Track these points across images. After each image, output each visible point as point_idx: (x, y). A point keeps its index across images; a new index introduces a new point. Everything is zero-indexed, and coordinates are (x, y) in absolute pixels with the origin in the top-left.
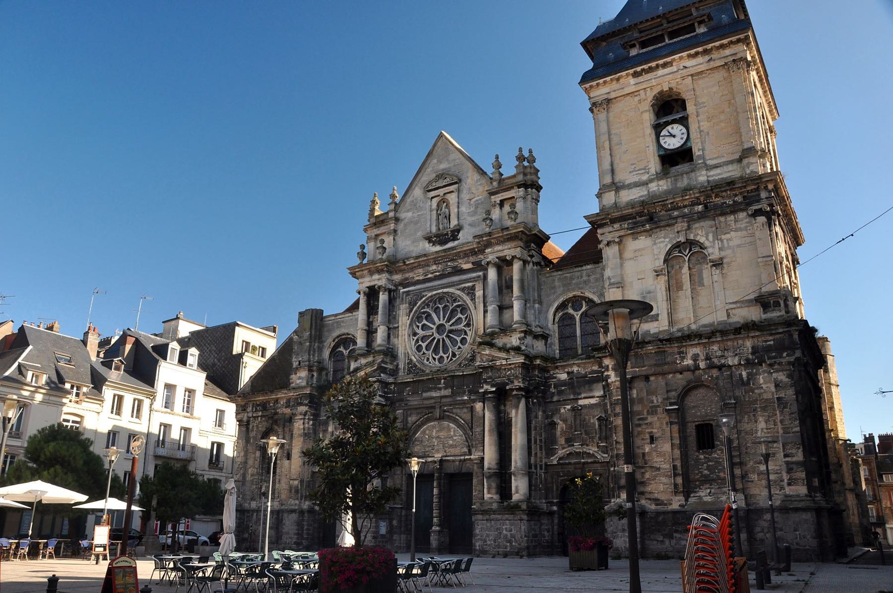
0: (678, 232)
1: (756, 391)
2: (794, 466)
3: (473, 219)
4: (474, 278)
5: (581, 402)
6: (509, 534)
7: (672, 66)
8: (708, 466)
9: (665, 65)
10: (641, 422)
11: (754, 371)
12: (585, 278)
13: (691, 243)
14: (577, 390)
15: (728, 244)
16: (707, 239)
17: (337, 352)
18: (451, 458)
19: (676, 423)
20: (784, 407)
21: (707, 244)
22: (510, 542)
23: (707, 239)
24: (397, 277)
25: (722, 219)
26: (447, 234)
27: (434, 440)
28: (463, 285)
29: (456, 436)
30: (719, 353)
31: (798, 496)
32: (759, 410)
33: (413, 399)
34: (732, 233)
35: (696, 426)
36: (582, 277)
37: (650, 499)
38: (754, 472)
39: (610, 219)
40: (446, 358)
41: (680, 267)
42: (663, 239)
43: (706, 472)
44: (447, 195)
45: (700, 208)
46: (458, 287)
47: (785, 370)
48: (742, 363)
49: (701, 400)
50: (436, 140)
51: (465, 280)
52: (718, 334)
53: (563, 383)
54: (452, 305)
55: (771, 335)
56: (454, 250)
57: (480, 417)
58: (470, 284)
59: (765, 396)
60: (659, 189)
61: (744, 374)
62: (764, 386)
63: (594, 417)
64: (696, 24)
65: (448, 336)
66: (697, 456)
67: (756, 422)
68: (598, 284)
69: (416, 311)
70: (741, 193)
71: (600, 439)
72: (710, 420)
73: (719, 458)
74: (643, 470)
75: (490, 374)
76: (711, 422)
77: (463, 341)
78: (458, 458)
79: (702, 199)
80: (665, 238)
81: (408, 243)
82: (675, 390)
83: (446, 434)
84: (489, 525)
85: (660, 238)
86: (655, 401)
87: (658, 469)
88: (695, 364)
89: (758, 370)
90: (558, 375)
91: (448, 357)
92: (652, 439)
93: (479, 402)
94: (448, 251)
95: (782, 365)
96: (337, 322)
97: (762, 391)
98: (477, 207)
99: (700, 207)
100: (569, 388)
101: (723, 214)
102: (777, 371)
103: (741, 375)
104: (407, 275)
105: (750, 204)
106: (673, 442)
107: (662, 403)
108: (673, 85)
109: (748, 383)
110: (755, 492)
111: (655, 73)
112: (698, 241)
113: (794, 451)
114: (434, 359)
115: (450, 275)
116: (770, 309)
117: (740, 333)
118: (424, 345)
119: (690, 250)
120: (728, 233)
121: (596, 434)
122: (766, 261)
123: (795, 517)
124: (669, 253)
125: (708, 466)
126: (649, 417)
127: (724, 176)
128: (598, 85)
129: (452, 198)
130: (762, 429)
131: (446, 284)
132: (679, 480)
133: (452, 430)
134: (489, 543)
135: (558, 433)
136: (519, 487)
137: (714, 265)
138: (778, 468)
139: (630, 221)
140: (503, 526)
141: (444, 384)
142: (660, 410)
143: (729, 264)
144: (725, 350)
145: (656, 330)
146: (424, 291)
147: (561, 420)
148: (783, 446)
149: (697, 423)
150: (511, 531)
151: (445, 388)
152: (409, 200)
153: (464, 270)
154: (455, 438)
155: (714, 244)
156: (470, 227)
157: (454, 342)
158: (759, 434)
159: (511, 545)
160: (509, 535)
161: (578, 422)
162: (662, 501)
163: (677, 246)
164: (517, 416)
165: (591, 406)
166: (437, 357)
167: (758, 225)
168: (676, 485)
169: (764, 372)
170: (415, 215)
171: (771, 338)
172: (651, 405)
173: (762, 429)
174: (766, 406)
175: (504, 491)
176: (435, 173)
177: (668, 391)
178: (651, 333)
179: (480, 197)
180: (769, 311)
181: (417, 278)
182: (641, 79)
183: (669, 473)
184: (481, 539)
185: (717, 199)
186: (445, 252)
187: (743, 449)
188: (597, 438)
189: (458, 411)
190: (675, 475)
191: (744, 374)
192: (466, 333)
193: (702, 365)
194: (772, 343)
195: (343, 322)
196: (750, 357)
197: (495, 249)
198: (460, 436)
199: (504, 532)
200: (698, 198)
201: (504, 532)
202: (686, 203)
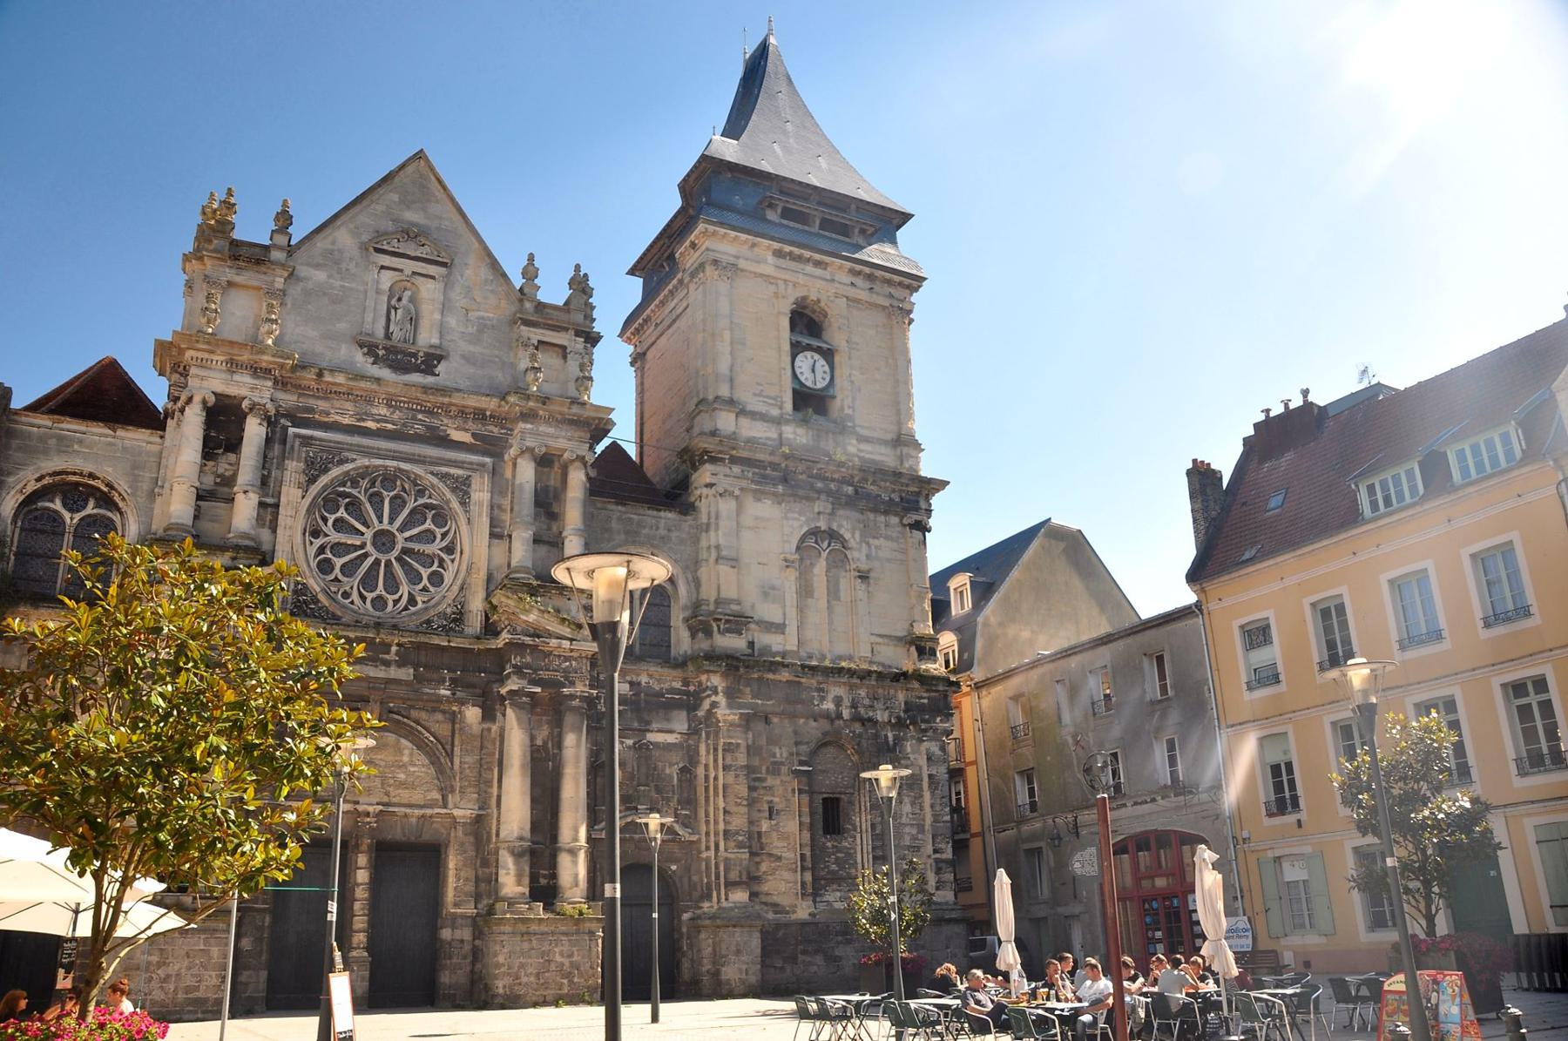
0: (819, 513)
2: (943, 865)
3: (472, 348)
4: (471, 463)
5: (652, 737)
6: (566, 962)
7: (825, 269)
8: (837, 858)
9: (818, 264)
10: (757, 784)
12: (662, 532)
13: (833, 535)
14: (646, 717)
16: (853, 537)
17: (36, 509)
19: (806, 792)
21: (852, 543)
22: (569, 976)
23: (853, 537)
24: (289, 399)
25: (871, 516)
26: (415, 355)
28: (444, 469)
29: (415, 765)
30: (867, 702)
36: (657, 528)
37: (766, 904)
39: (731, 456)
40: (390, 604)
41: (811, 564)
42: (796, 515)
43: (834, 867)
44: (417, 277)
45: (850, 490)
46: (432, 468)
48: (893, 721)
50: (410, 159)
51: (450, 461)
54: (416, 500)
55: (927, 691)
56: (445, 396)
57: (473, 736)
58: (459, 472)
60: (795, 439)
61: (890, 735)
63: (671, 765)
65: (398, 559)
66: (824, 843)
68: (683, 548)
69: (325, 488)
70: (900, 491)
71: (679, 802)
72: (840, 793)
75: (529, 659)
76: (843, 796)
77: (437, 579)
79: (856, 479)
81: (312, 333)
82: (807, 743)
83: (390, 758)
84: (526, 946)
85: (793, 512)
86: (778, 755)
87: (779, 858)
89: (905, 734)
91: (396, 602)
92: (772, 813)
93: (473, 705)
94: (433, 394)
96: (61, 438)
97: (909, 762)
98: (481, 331)
99: (850, 488)
101: (875, 510)
102: (930, 740)
103: (886, 736)
104: (312, 402)
105: (907, 510)
107: (787, 759)
108: (823, 298)
111: (802, 266)
112: (842, 536)
114: (363, 598)
115: (417, 439)
118: (339, 562)
119: (829, 545)
120: (877, 538)
121: (674, 793)
123: (947, 930)
124: (803, 539)
125: (837, 858)
126: (769, 777)
127: (877, 458)
128: (736, 238)
129: (429, 291)
131: (406, 453)
132: (808, 877)
133: (406, 752)
134: (524, 980)
137: (860, 577)
139: (757, 470)
140: (556, 945)
141: (396, 654)
142: (784, 769)
144: (875, 699)
146: (349, 450)
149: (825, 796)
150: (571, 956)
151: (401, 664)
152: (321, 243)
153: (452, 441)
154: (412, 769)
155: (861, 547)
157: (414, 578)
159: (571, 982)
160: (567, 964)
161: (643, 770)
162: (783, 907)
163: (815, 533)
164: (575, 749)
165: (668, 747)
166: (370, 596)
167: (914, 540)
168: (803, 884)
169: (912, 737)
170: (338, 283)
171: (925, 695)
172: (772, 759)
176: (393, 221)
177: (797, 744)
179: (491, 315)
181: (338, 418)
182: (781, 262)
183: (794, 866)
184: (508, 974)
185: (872, 487)
186: (425, 393)
188: (675, 800)
189: (423, 715)
190: (803, 869)
192: (441, 563)
193: (846, 714)
194: (926, 701)
195: (80, 442)
196: (902, 714)
197: (541, 429)
199: (558, 958)
200: (852, 477)
202: (836, 476)
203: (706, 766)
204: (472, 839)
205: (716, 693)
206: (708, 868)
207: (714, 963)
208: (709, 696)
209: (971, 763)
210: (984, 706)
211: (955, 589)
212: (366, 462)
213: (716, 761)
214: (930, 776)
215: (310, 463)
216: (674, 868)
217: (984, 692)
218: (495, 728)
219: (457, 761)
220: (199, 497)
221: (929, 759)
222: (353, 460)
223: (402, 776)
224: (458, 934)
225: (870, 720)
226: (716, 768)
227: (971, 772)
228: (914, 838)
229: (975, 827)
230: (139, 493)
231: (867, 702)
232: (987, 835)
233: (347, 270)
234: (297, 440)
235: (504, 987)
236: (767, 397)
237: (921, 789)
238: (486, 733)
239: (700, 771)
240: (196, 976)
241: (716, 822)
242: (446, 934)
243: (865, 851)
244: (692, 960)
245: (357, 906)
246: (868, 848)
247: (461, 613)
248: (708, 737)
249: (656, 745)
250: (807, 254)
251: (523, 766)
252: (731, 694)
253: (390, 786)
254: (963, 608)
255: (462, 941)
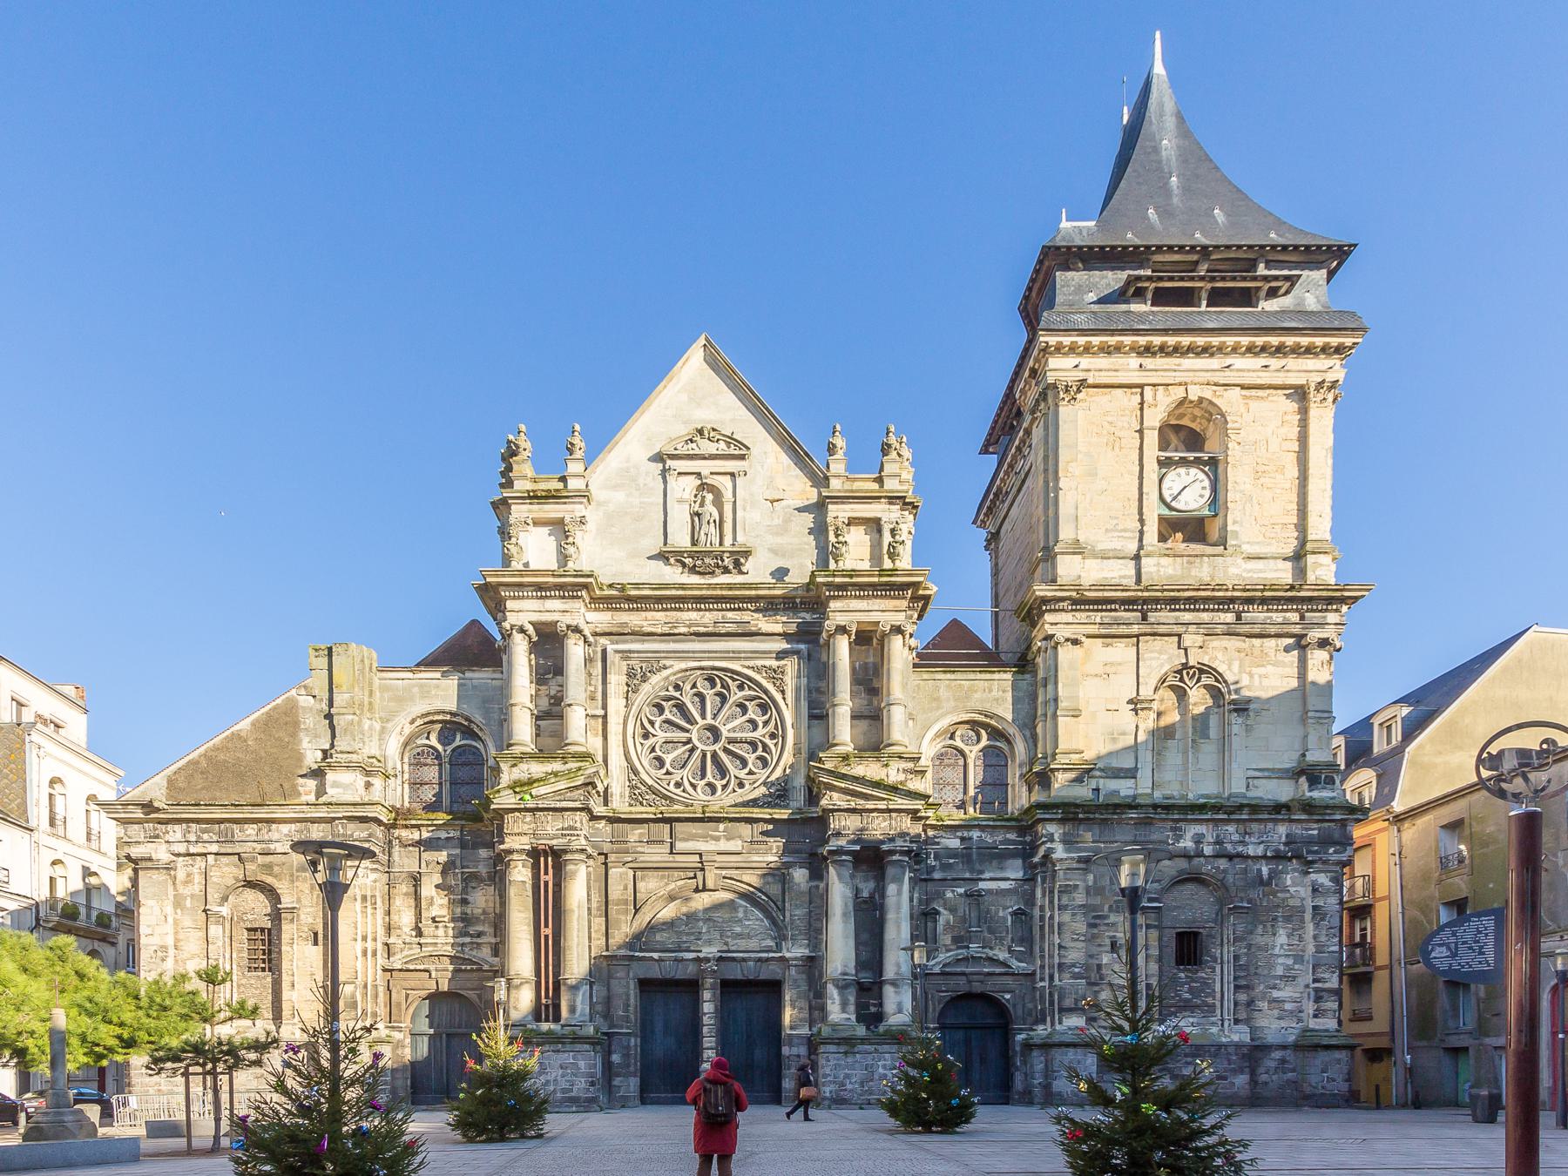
1: (1279, 895)
3: (779, 540)
5: (982, 885)
10: (1098, 921)
11: (1280, 867)
15: (1261, 683)
16: (1230, 669)
18: (741, 955)
19: (1155, 927)
20: (1323, 919)
23: (1230, 669)
27: (701, 924)
29: (749, 920)
30: (1236, 837)
31: (1327, 1031)
32: (1280, 919)
33: (650, 851)
34: (1269, 667)
35: (1179, 934)
36: (991, 691)
38: (1263, 999)
42: (1156, 655)
46: (747, 663)
47: (1330, 872)
49: (1188, 899)
52: (1246, 810)
53: (953, 853)
59: (1291, 902)
61: (1265, 870)
62: (1292, 890)
63: (1005, 908)
64: (1263, 294)
65: (726, 750)
67: (1275, 935)
71: (1013, 940)
73: (1208, 979)
74: (1096, 988)
76: (1201, 930)
78: (753, 955)
80: (1160, 653)
83: (727, 916)
85: (1152, 652)
88: (1197, 848)
90: (943, 840)
95: (1328, 864)
96: (421, 686)
97: (1288, 895)
100: (963, 863)
103: (1260, 871)
106: (1149, 952)
109: (1269, 883)
110: (1262, 1024)
113: (1326, 976)
116: (1320, 786)
117: (1279, 813)
120: (1263, 666)
121: (1007, 933)
122: (1320, 718)
126: (1112, 915)
130: (1282, 945)
133: (741, 910)
135: (940, 928)
136: (899, 1006)
137: (1236, 710)
138: (1298, 995)
143: (1257, 713)
144: (1246, 833)
145: (1131, 792)
147: (945, 909)
148: (1313, 968)
149: (1179, 930)
156: (772, 555)
158: (1277, 951)
169: (1294, 870)
171: (1315, 826)
173: (1282, 945)
174: (1291, 916)
175: (871, 1015)
176: (684, 423)
178: (1122, 794)
180: (1317, 789)
182: (1149, 362)
187: (1252, 970)
191: (1265, 870)
193: (1208, 850)
194: (1315, 832)
196: (1282, 847)
198: (757, 920)
199: (881, 1070)
201: (881, 1070)
203: (1042, 908)
204: (804, 976)
205: (1052, 840)
206: (1042, 997)
207: (1046, 1077)
208: (1044, 843)
209: (1382, 899)
210: (1404, 839)
211: (1381, 724)
212: (683, 665)
213: (1051, 902)
214: (1315, 908)
215: (631, 675)
216: (1008, 996)
217: (1407, 825)
218: (822, 885)
219: (787, 914)
220: (538, 718)
221: (1315, 890)
222: (671, 666)
223: (738, 929)
224: (795, 1051)
225: (1239, 855)
226: (1052, 909)
227: (1381, 912)
228: (1288, 968)
229: (1381, 958)
230: (492, 723)
231: (1236, 837)
232: (1396, 966)
233: (645, 485)
234: (617, 655)
235: (831, 1092)
236: (1125, 530)
237: (1302, 921)
238: (813, 890)
239: (1037, 912)
240: (568, 1081)
241: (1051, 956)
242: (785, 1050)
243: (1225, 980)
244: (1026, 1074)
245: (705, 1029)
246: (1229, 976)
247: (785, 790)
248: (1043, 882)
249: (990, 892)
250: (1186, 340)
251: (845, 915)
252: (1068, 842)
253: (728, 937)
254: (1389, 742)
255: (799, 1056)
